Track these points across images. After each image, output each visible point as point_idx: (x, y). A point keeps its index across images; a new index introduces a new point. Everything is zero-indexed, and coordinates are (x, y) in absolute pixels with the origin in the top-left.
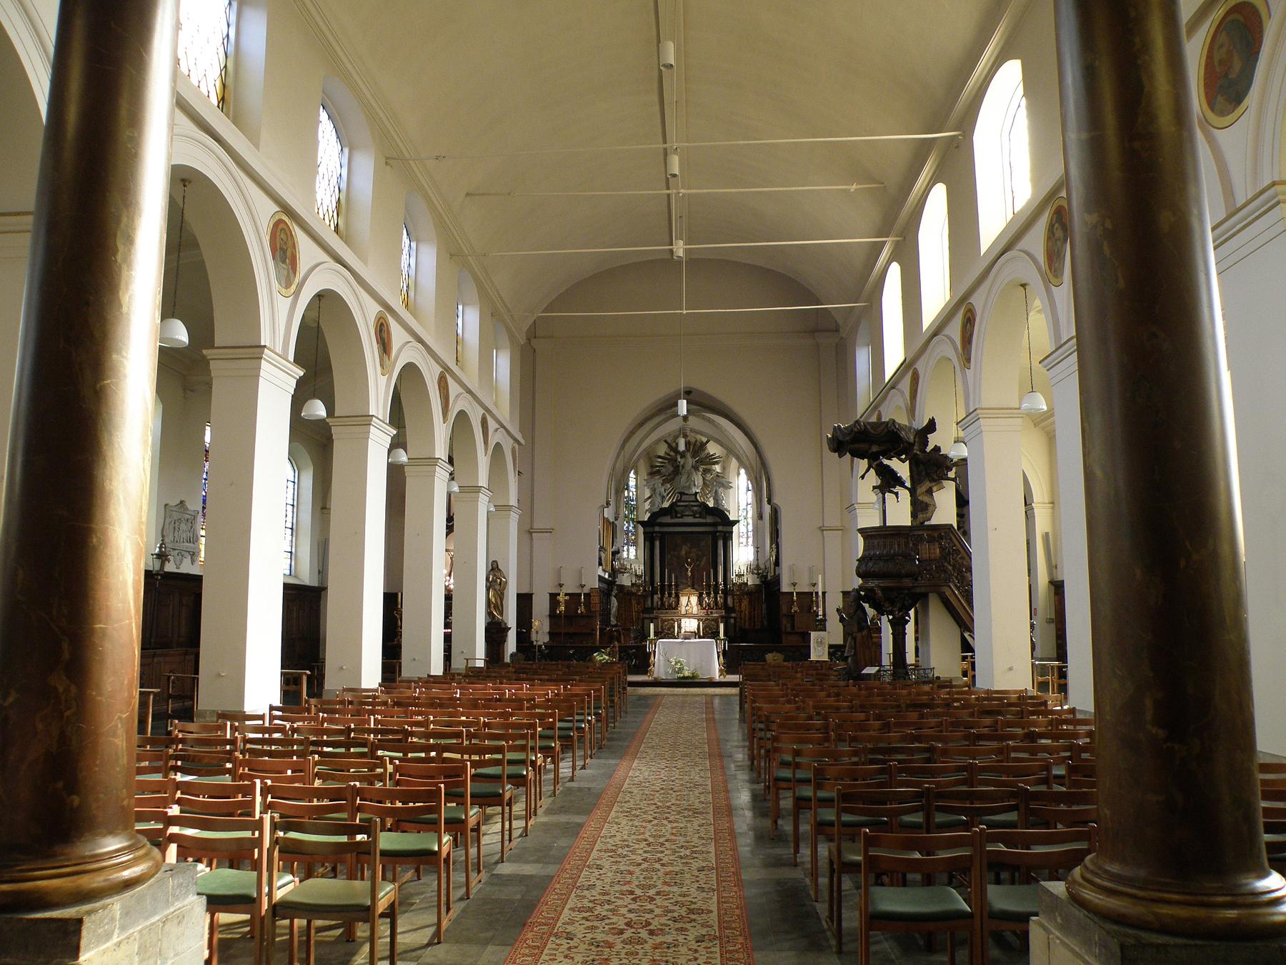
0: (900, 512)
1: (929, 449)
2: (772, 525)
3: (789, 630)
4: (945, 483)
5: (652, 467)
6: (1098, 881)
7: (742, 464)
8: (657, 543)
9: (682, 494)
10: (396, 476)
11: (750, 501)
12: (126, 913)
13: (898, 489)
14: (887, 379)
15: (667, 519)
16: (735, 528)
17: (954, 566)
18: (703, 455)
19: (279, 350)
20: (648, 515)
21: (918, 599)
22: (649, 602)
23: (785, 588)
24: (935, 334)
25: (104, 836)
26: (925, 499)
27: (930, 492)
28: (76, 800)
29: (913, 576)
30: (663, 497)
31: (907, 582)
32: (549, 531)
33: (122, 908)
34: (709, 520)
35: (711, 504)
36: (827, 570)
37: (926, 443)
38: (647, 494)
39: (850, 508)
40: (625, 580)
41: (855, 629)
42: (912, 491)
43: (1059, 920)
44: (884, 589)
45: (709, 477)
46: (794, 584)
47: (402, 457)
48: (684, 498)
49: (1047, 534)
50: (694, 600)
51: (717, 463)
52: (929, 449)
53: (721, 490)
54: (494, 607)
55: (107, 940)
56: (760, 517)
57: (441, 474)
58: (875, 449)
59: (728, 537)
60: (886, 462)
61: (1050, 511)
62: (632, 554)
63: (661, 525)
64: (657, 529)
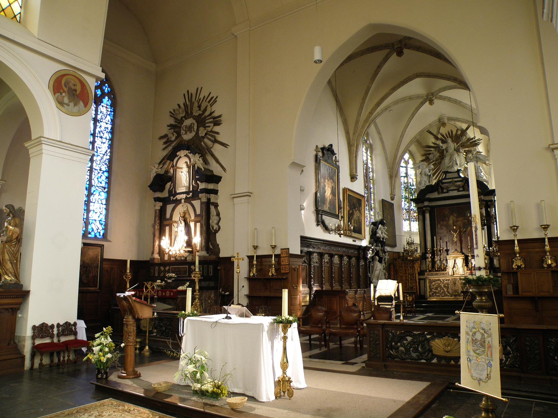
3: (510, 293)
8: (427, 216)
9: (446, 173)
15: (435, 195)
22: (424, 266)
32: (248, 195)
48: (449, 176)
50: (460, 261)
63: (431, 200)
64: (426, 203)
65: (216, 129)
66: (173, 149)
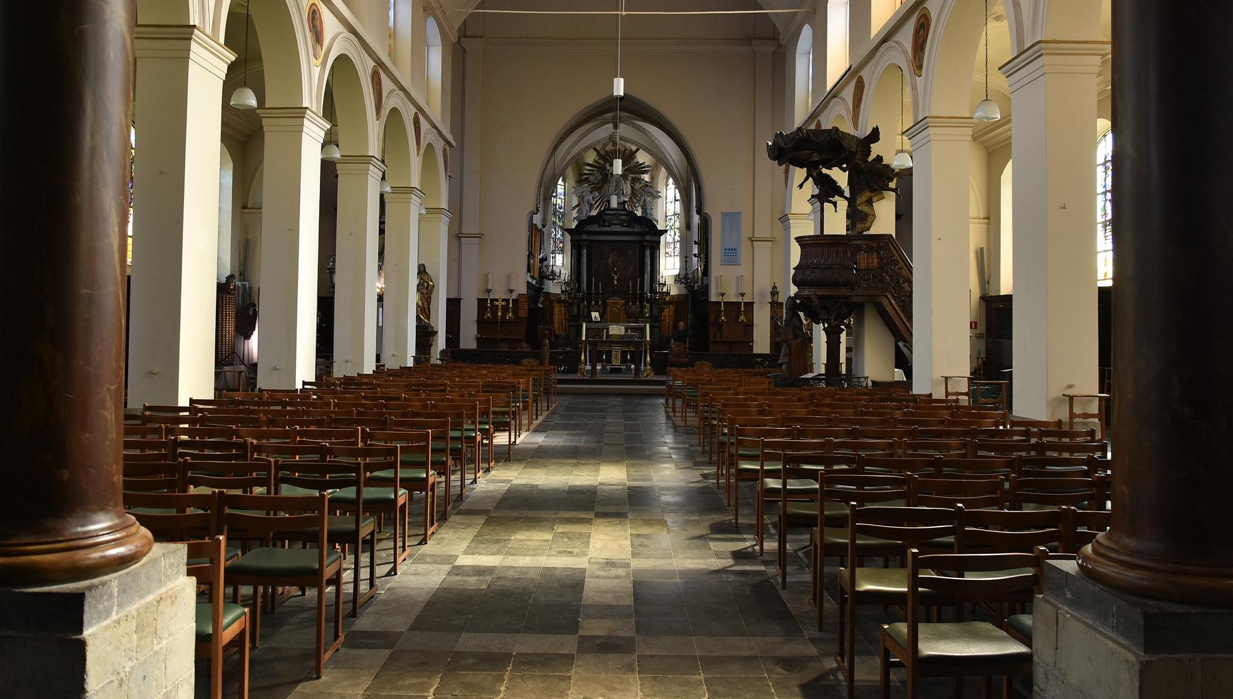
0: (836, 222)
1: (871, 159)
2: (699, 239)
4: (886, 193)
5: (581, 174)
6: (1115, 556)
7: (671, 173)
10: (329, 171)
11: (678, 210)
12: (123, 591)
13: (837, 198)
14: (829, 87)
15: (595, 228)
16: (662, 238)
17: (891, 277)
18: (632, 164)
19: (208, 31)
20: (576, 223)
21: (857, 309)
23: (713, 298)
24: (885, 40)
25: (95, 512)
26: (865, 209)
27: (870, 202)
28: (66, 475)
29: (850, 285)
30: (591, 205)
31: (844, 291)
32: (479, 236)
33: (119, 585)
34: (637, 229)
35: (639, 213)
36: (760, 276)
37: (869, 152)
38: (575, 203)
39: (784, 219)
40: (553, 288)
41: (791, 336)
42: (851, 202)
43: (1069, 595)
44: (821, 298)
45: (638, 186)
46: (723, 295)
47: (336, 154)
49: (982, 249)
51: (645, 172)
52: (871, 159)
53: (649, 199)
54: (424, 309)
55: (107, 617)
56: (688, 226)
57: (374, 173)
58: (815, 157)
59: (655, 247)
60: (824, 171)
61: (985, 226)
62: (560, 262)
64: (584, 237)
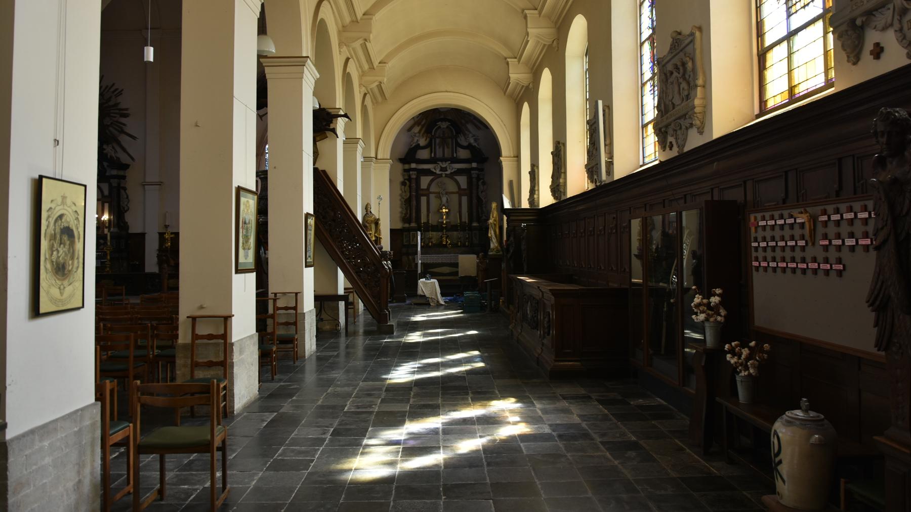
64: (413, 166)
65: (123, 120)
66: (486, 450)
